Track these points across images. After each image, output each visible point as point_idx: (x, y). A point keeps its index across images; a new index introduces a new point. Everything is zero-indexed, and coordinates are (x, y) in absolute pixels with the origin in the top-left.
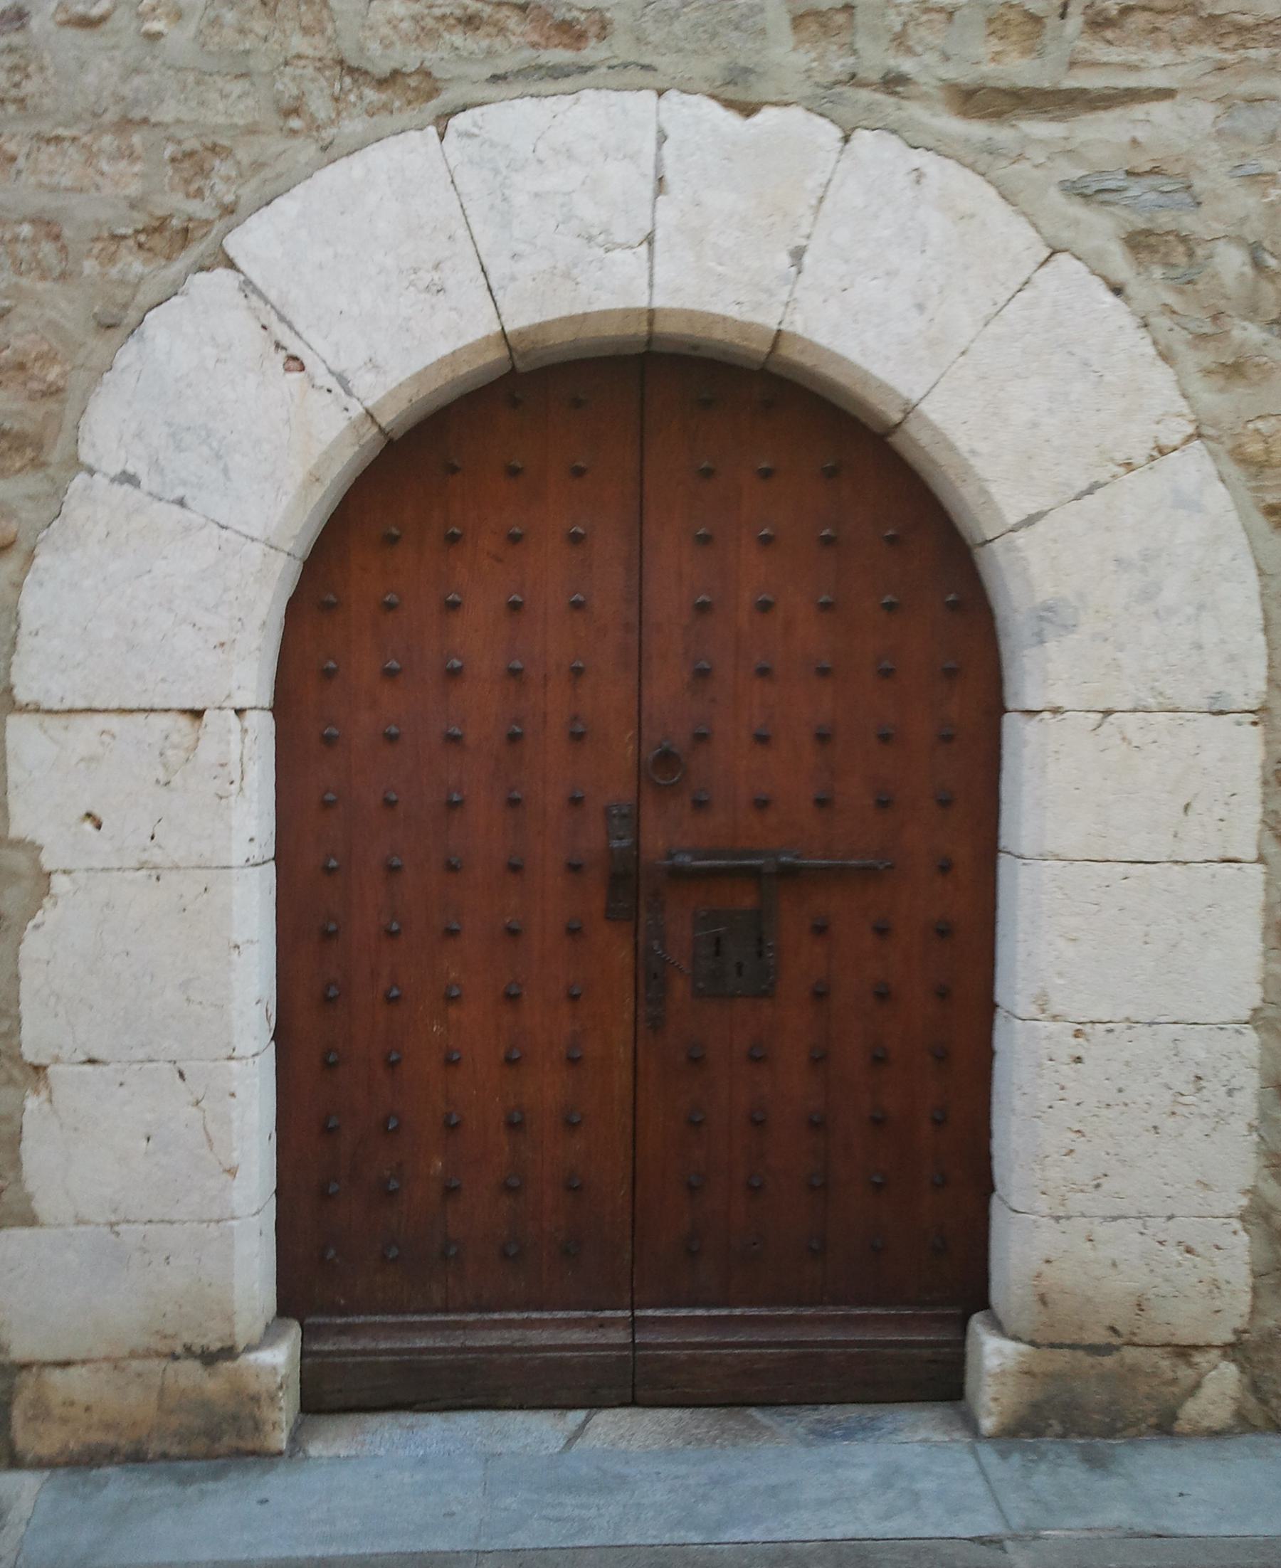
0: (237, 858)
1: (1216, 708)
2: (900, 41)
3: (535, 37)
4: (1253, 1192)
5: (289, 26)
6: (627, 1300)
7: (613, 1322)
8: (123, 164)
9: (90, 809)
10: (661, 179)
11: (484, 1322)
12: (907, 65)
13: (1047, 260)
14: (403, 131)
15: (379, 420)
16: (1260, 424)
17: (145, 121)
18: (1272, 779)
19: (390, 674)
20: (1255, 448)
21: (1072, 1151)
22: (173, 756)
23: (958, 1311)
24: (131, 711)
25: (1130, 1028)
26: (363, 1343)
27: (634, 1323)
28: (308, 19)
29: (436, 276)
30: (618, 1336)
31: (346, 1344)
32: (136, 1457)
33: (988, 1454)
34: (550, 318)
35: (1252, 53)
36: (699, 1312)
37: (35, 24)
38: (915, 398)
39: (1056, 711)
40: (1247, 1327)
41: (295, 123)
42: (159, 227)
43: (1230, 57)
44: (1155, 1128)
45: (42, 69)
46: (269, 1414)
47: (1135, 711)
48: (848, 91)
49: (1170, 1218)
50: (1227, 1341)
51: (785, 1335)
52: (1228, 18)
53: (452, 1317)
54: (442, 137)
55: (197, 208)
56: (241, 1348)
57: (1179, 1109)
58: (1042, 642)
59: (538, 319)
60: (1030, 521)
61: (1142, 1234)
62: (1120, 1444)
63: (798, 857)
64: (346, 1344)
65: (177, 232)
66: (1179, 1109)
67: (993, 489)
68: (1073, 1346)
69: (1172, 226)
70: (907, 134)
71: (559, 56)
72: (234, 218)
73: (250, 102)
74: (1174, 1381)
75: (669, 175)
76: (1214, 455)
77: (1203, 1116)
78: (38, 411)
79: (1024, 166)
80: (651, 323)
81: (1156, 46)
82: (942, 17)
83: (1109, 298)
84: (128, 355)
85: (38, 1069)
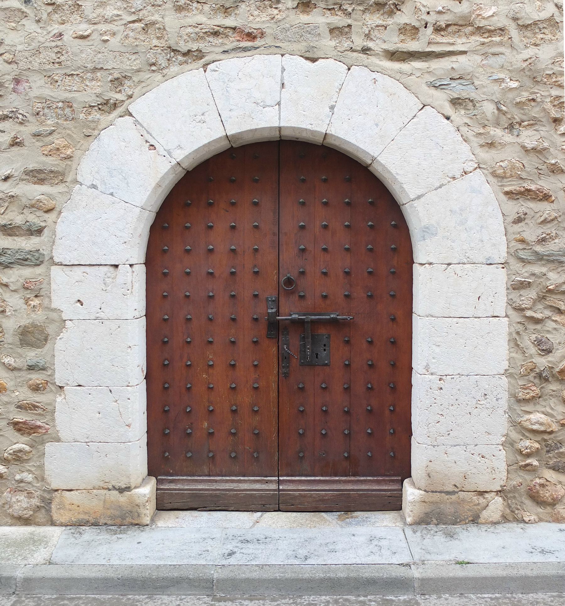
0: (129, 316)
1: (488, 262)
2: (368, 36)
3: (238, 38)
4: (507, 435)
5: (152, 36)
6: (277, 473)
7: (271, 481)
8: (94, 82)
9: (79, 299)
10: (283, 84)
11: (224, 480)
12: (370, 44)
13: (422, 108)
14: (191, 70)
15: (182, 165)
16: (501, 164)
17: (102, 68)
18: (510, 287)
19: (188, 251)
20: (500, 171)
21: (439, 422)
22: (108, 281)
23: (400, 478)
24: (94, 265)
25: (459, 377)
26: (179, 486)
27: (279, 482)
28: (158, 35)
29: (203, 117)
30: (274, 486)
31: (173, 486)
32: (95, 524)
33: (409, 531)
34: (243, 130)
35: (494, 39)
36: (303, 478)
37: (65, 38)
38: (375, 156)
39: (430, 264)
40: (505, 484)
41: (154, 68)
42: (107, 103)
43: (486, 40)
44: (470, 413)
45: (67, 52)
46: (142, 511)
47: (459, 263)
48: (349, 53)
49: (476, 445)
50: (498, 490)
51: (335, 487)
52: (485, 28)
53: (212, 478)
54: (205, 71)
55: (120, 97)
56: (133, 488)
57: (478, 406)
58: (424, 240)
59: (239, 131)
60: (419, 197)
61: (465, 451)
62: (459, 527)
63: (338, 315)
64: (173, 486)
65: (112, 104)
66: (478, 406)
67: (405, 186)
68: (441, 492)
69: (468, 97)
70: (370, 67)
71: (249, 44)
72: (132, 99)
73: (138, 61)
74: (479, 504)
75: (286, 83)
76: (486, 175)
77: (487, 408)
78: (63, 164)
79: (412, 77)
80: (280, 131)
81: (460, 36)
82: (383, 28)
83: (446, 121)
84: (94, 145)
85: (61, 387)
